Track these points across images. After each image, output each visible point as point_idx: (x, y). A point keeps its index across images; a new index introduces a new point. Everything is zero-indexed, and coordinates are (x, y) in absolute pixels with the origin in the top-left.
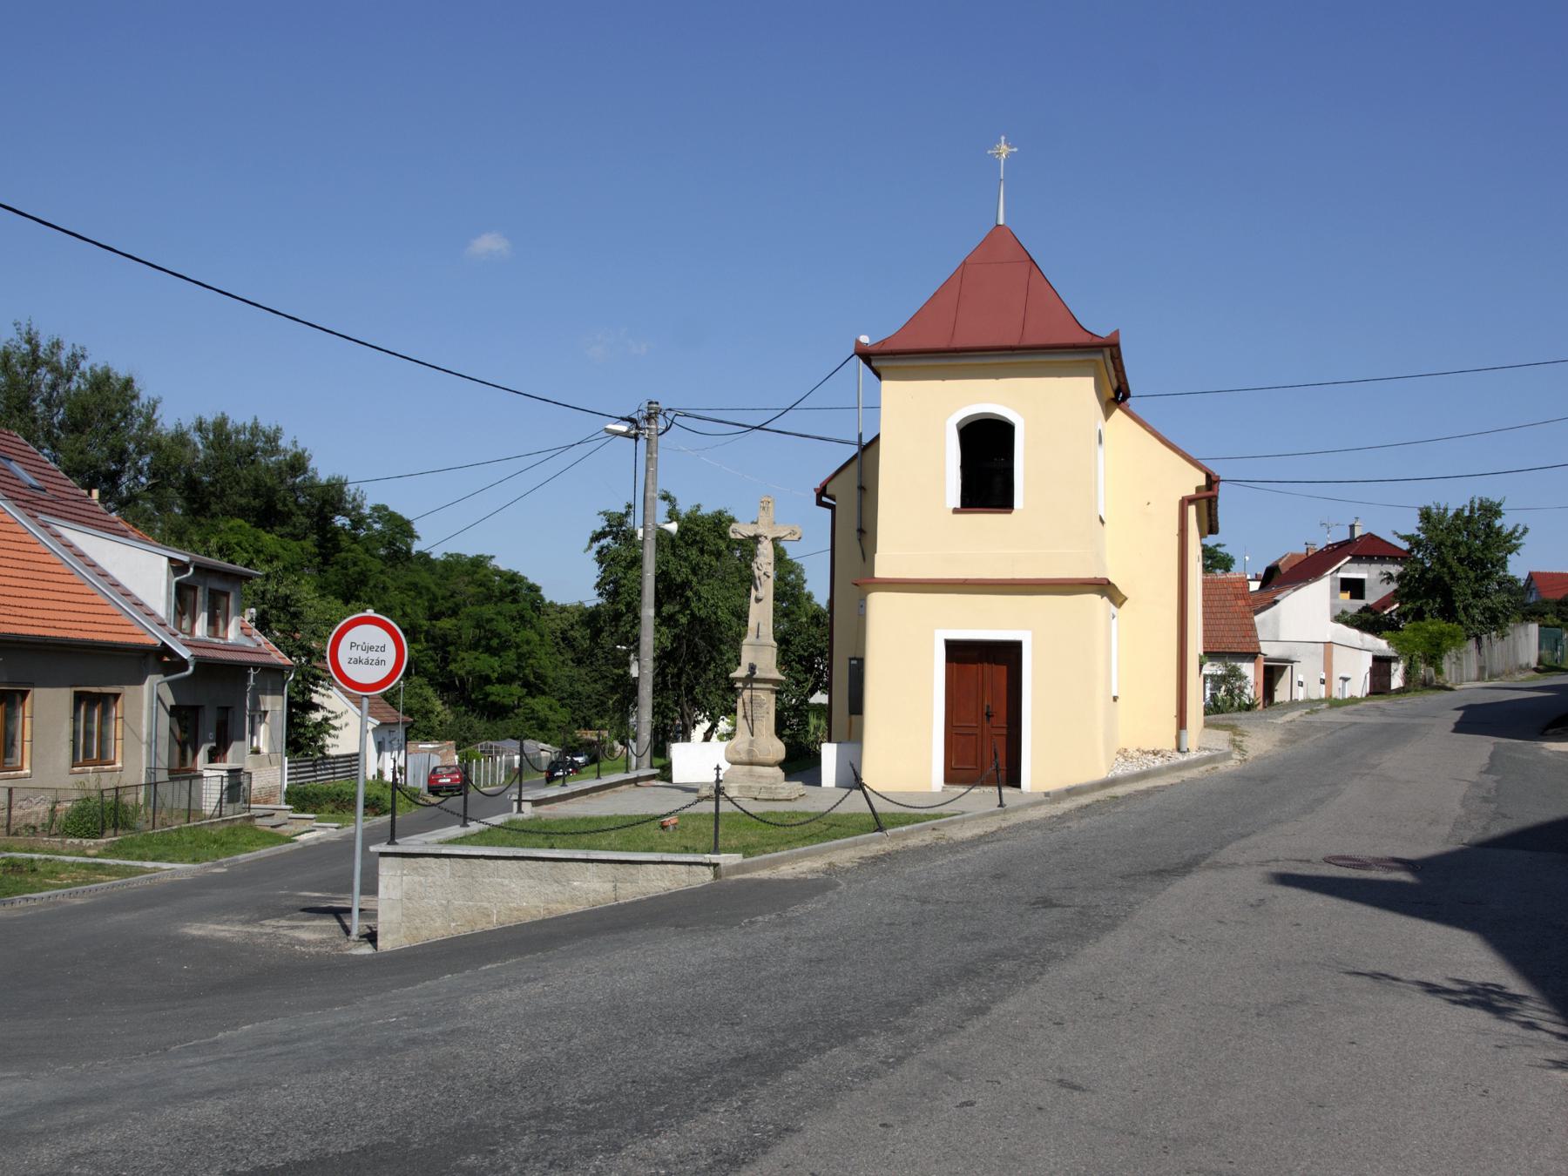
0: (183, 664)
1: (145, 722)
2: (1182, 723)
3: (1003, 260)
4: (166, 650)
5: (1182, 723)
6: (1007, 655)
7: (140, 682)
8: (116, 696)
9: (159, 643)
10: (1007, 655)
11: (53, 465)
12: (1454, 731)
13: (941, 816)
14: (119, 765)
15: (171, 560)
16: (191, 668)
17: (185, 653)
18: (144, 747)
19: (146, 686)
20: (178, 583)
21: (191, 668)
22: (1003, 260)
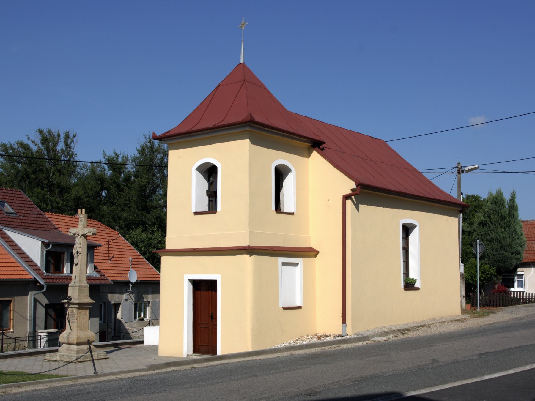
0: (42, 287)
1: (28, 311)
2: (344, 321)
3: (242, 79)
4: (35, 281)
5: (344, 321)
6: (212, 285)
7: (26, 294)
8: (10, 301)
9: (33, 278)
10: (212, 285)
11: (29, 199)
12: (490, 193)
13: (57, 376)
14: (12, 330)
15: (42, 242)
16: (45, 288)
17: (42, 282)
18: (28, 322)
19: (29, 296)
20: (47, 252)
21: (45, 288)
22: (242, 79)
